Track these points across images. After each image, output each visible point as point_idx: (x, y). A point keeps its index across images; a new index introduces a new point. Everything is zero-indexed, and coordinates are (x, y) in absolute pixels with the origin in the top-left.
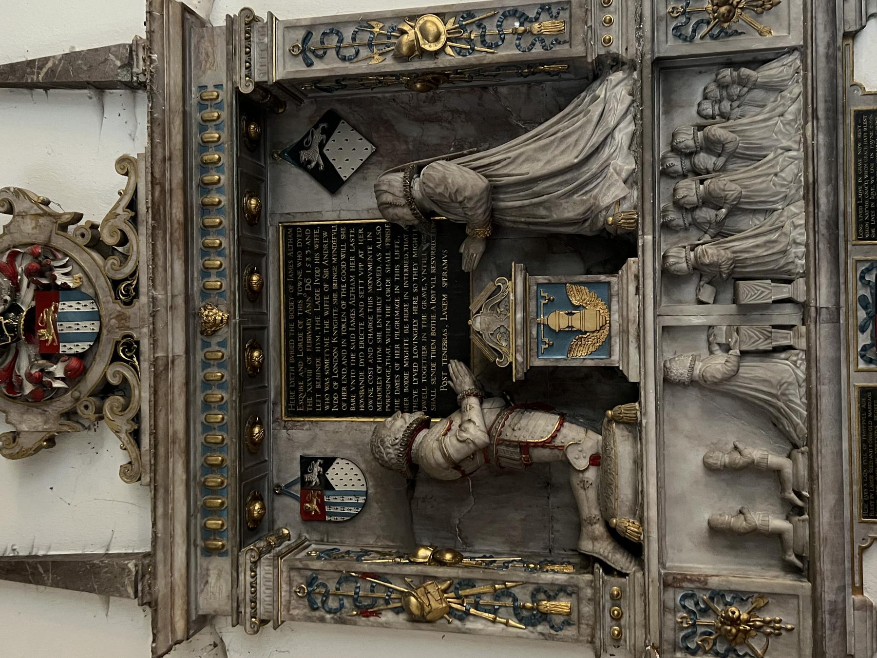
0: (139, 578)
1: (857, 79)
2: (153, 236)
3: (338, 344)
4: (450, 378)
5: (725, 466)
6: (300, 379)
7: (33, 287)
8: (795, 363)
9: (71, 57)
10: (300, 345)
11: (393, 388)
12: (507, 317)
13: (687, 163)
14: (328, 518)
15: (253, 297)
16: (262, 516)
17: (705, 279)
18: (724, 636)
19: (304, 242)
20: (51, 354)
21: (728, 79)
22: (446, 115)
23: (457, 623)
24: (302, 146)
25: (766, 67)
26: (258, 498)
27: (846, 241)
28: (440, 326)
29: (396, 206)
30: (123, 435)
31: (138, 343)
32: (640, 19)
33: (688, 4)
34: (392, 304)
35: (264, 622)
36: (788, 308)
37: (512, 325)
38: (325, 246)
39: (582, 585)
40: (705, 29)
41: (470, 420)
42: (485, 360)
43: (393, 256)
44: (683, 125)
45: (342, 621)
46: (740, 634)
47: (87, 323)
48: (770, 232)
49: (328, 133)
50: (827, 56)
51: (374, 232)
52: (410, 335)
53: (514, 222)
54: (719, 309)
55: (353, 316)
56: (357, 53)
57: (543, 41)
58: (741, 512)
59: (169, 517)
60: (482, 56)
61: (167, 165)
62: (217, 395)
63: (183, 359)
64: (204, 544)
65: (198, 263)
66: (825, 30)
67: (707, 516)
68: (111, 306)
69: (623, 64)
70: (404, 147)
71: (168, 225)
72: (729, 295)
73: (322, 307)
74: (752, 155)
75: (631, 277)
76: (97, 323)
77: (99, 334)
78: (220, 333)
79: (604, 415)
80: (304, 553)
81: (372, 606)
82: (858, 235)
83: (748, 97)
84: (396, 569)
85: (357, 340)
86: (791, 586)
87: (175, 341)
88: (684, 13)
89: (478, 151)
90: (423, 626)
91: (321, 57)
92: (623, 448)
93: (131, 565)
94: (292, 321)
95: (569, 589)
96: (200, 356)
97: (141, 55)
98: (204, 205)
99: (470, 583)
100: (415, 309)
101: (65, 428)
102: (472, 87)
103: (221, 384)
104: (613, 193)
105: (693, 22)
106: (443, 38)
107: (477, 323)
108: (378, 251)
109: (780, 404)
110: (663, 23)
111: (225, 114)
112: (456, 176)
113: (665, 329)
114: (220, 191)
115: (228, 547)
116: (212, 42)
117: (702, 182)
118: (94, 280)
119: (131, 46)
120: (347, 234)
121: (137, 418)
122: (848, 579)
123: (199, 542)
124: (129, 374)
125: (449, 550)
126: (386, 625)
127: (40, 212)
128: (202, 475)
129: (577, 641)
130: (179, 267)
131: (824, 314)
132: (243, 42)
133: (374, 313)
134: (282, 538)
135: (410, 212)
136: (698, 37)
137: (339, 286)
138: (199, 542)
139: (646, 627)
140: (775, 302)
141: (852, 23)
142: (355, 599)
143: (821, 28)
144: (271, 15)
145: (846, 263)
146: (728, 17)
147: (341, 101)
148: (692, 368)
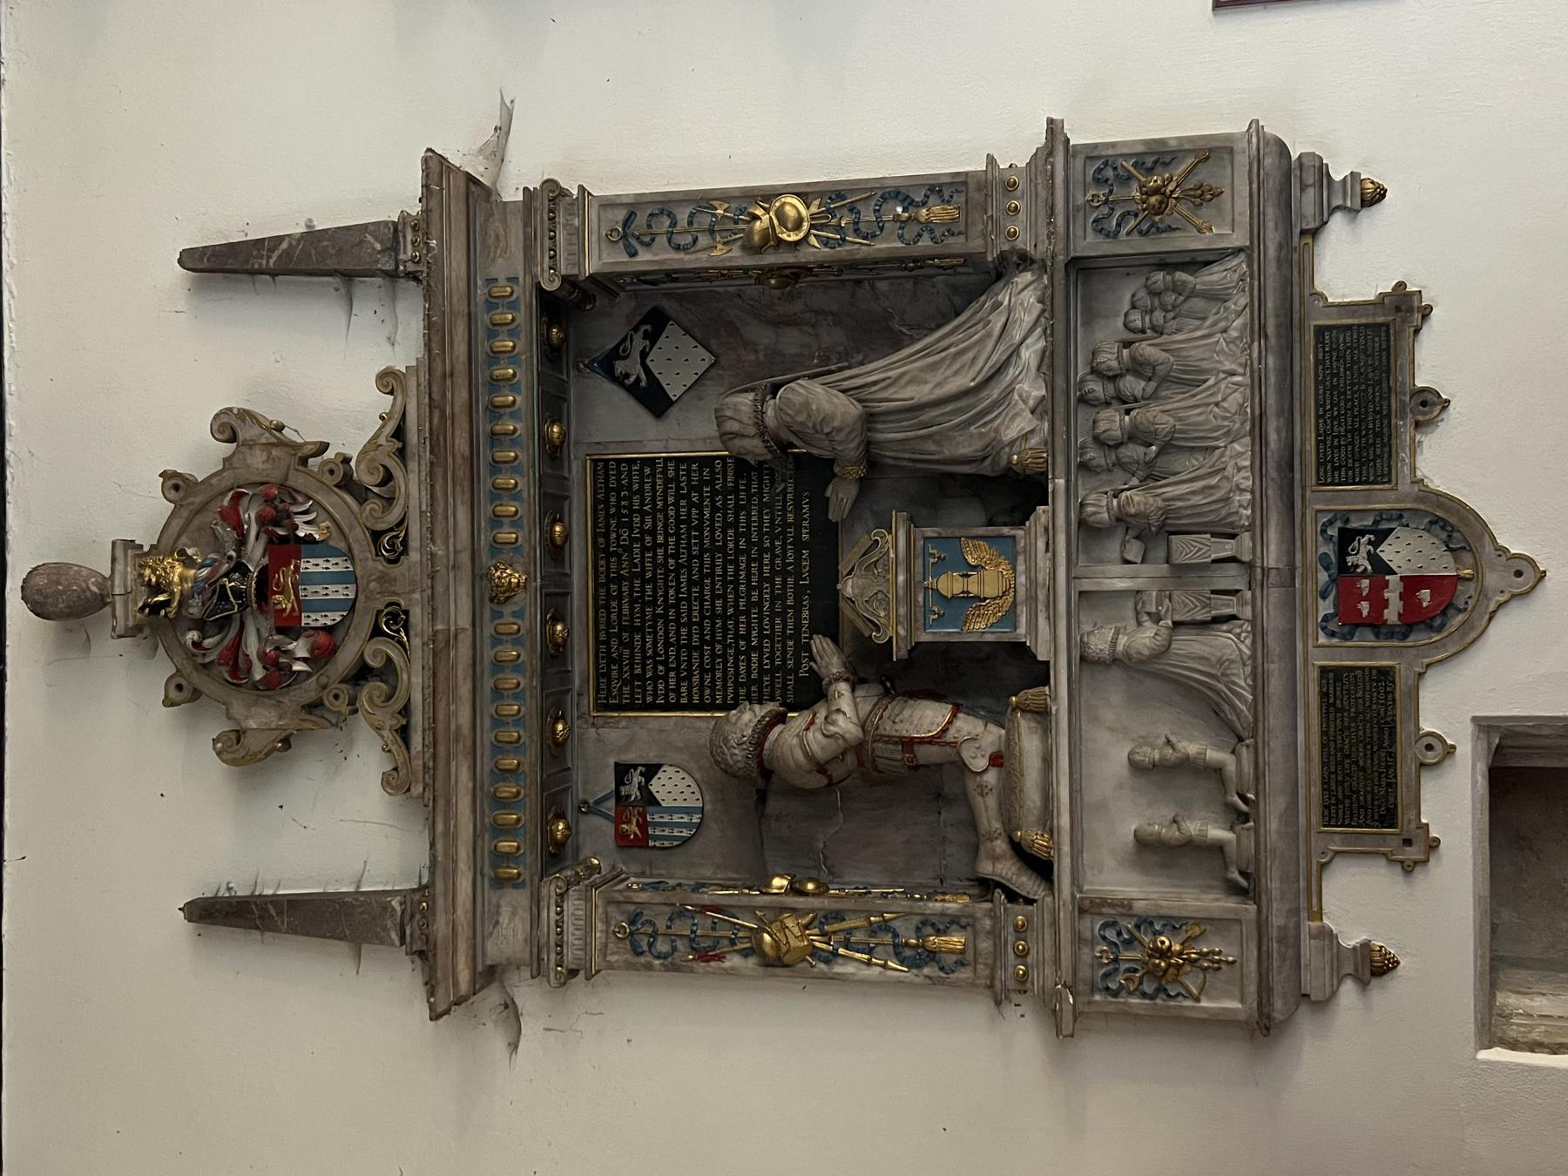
0: (407, 918)
1: (1319, 287)
3: (665, 616)
4: (812, 659)
6: (614, 661)
7: (264, 538)
8: (1238, 636)
9: (312, 237)
10: (614, 617)
11: (737, 673)
12: (886, 578)
14: (651, 843)
15: (556, 552)
17: (1132, 533)
18: (1152, 973)
19: (619, 480)
20: (289, 627)
21: (1160, 284)
22: (807, 316)
23: (822, 966)
24: (616, 354)
26: (560, 816)
27: (1303, 488)
28: (799, 592)
30: (386, 733)
31: (406, 612)
32: (1052, 212)
33: (1111, 192)
34: (736, 562)
35: (573, 973)
36: (1233, 569)
38: (647, 487)
39: (979, 915)
40: (1132, 223)
41: (839, 710)
43: (737, 500)
45: (675, 968)
46: (1171, 970)
47: (339, 587)
48: (1210, 475)
49: (653, 338)
50: (1279, 261)
51: (713, 467)
52: (760, 604)
53: (895, 459)
54: (1148, 570)
55: (683, 578)
56: (695, 240)
59: (451, 837)
60: (855, 247)
61: (449, 382)
62: (510, 680)
63: (469, 633)
64: (496, 875)
65: (486, 510)
66: (1276, 229)
67: (1133, 828)
69: (1033, 261)
70: (752, 357)
71: (450, 460)
72: (1161, 553)
73: (643, 567)
74: (1190, 379)
75: (1040, 530)
76: (352, 587)
77: (355, 600)
78: (515, 599)
82: (1318, 479)
83: (1186, 306)
84: (745, 901)
85: (690, 610)
86: (1232, 910)
87: (460, 612)
88: (1106, 202)
89: (850, 367)
90: (779, 971)
91: (647, 245)
92: (1030, 743)
94: (602, 585)
95: (963, 921)
96: (488, 630)
98: (493, 433)
99: (838, 916)
100: (766, 569)
102: (843, 282)
104: (1018, 427)
105: (1118, 213)
106: (806, 226)
107: (849, 588)
108: (718, 493)
109: (1221, 686)
110: (1081, 215)
111: (521, 317)
112: (821, 400)
113: (1082, 594)
114: (514, 416)
115: (526, 875)
116: (504, 221)
117: (1128, 412)
118: (347, 531)
120: (677, 470)
121: (406, 711)
122: (1303, 903)
123: (487, 869)
125: (811, 880)
126: (733, 973)
127: (273, 440)
129: (974, 985)
130: (462, 515)
132: (547, 223)
133: (712, 575)
135: (761, 444)
136: (1124, 232)
137: (666, 538)
138: (487, 869)
139: (1057, 962)
140: (1214, 561)
141: (1311, 219)
142: (692, 940)
143: (1271, 225)
144: (582, 189)
145: (1304, 514)
146: (1159, 210)
147: (669, 295)
148: (1114, 643)
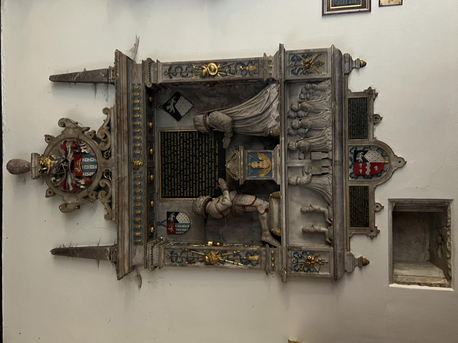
2: (117, 136)
3: (180, 173)
4: (219, 184)
5: (307, 211)
6: (167, 185)
7: (72, 153)
8: (329, 178)
9: (86, 73)
10: (166, 173)
12: (238, 163)
13: (296, 114)
15: (151, 156)
16: (154, 232)
18: (306, 265)
20: (79, 176)
21: (309, 87)
23: (221, 265)
25: (320, 83)
26: (152, 226)
27: (345, 140)
28: (215, 166)
29: (201, 126)
30: (105, 204)
31: (111, 172)
34: (199, 159)
35: (155, 267)
36: (327, 161)
37: (239, 166)
38: (175, 139)
39: (262, 251)
40: (301, 71)
41: (226, 198)
42: (230, 178)
44: (294, 102)
45: (183, 266)
46: (312, 265)
47: (93, 166)
49: (177, 100)
50: (339, 81)
52: (205, 170)
55: (185, 163)
56: (188, 74)
57: (250, 73)
58: (312, 226)
59: (123, 232)
60: (230, 77)
62: (139, 190)
63: (128, 178)
64: (135, 241)
67: (302, 228)
68: (101, 160)
69: (276, 81)
70: (203, 105)
71: (122, 132)
72: (309, 157)
74: (316, 112)
76: (96, 166)
79: (269, 196)
80: (168, 244)
81: (193, 260)
83: (315, 93)
84: (201, 248)
88: (295, 65)
89: (228, 108)
91: (175, 76)
92: (275, 206)
93: (108, 249)
96: (133, 177)
97: (111, 73)
98: (134, 125)
99: (225, 251)
100: (207, 161)
101: (84, 202)
103: (140, 186)
104: (272, 124)
105: (298, 68)
106: (217, 71)
107: (228, 166)
109: (324, 191)
110: (288, 69)
111: (141, 94)
112: (221, 116)
114: (140, 120)
115: (143, 242)
116: (137, 69)
117: (300, 120)
119: (108, 70)
121: (111, 198)
122: (345, 247)
124: (108, 184)
125: (218, 242)
126: (197, 267)
127: (75, 126)
128: (134, 217)
129: (260, 269)
131: (337, 163)
133: (192, 162)
134: (161, 240)
136: (299, 73)
140: (323, 159)
142: (187, 258)
143: (337, 72)
144: (157, 61)
145: (345, 147)
146: (308, 68)
148: (297, 180)
